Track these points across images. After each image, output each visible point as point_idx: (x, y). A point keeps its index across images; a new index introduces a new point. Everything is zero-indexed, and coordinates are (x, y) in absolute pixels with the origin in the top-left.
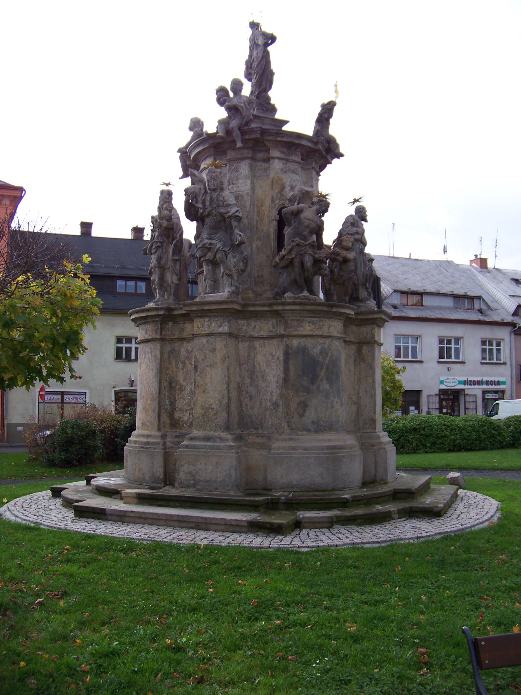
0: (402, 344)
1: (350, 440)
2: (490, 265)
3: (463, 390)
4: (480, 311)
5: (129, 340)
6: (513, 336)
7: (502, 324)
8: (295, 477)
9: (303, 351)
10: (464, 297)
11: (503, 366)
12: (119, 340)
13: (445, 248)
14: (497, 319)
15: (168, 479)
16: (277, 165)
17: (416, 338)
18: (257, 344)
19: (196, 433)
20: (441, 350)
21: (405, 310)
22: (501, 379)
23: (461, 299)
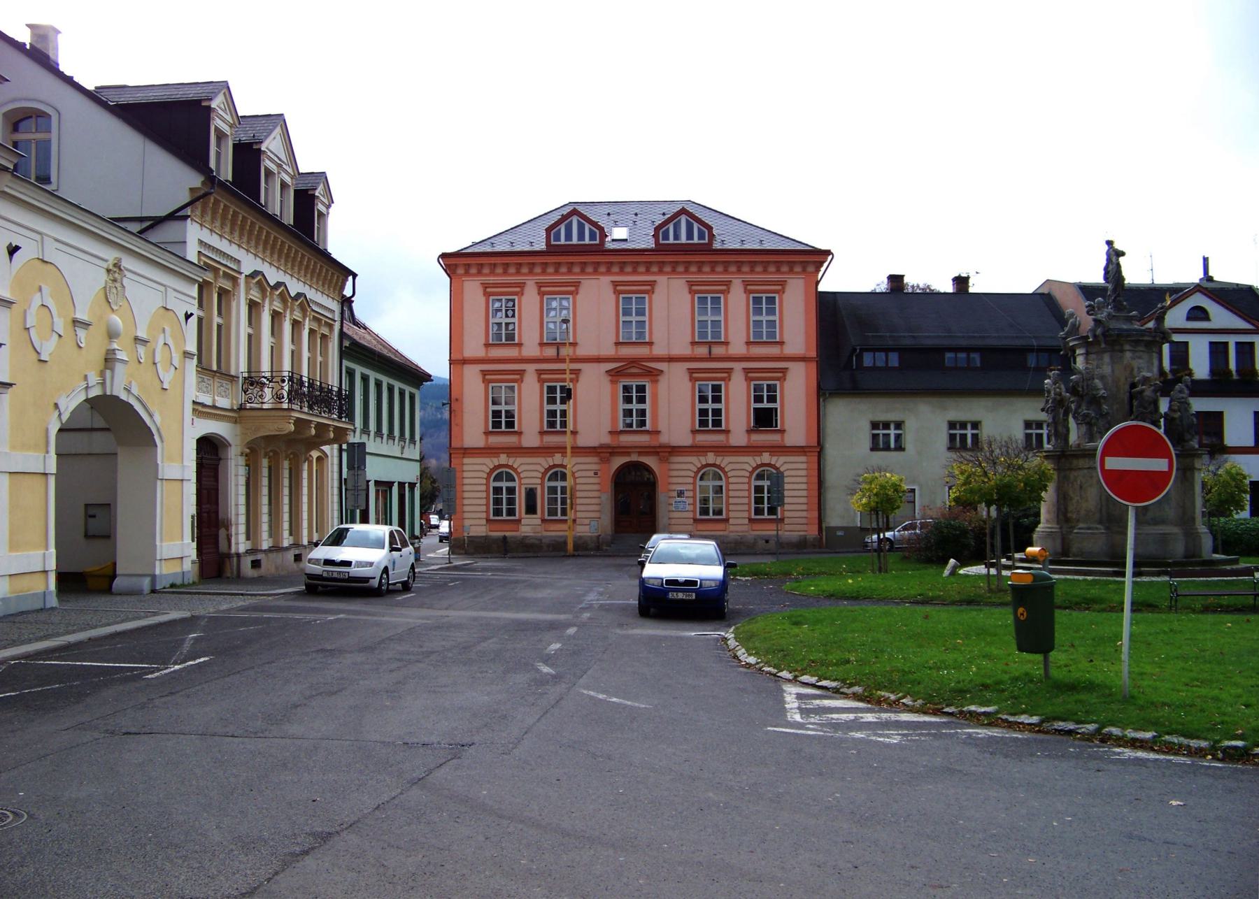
1: (1175, 530)
12: (875, 425)
15: (1065, 552)
16: (1128, 355)
19: (1081, 525)
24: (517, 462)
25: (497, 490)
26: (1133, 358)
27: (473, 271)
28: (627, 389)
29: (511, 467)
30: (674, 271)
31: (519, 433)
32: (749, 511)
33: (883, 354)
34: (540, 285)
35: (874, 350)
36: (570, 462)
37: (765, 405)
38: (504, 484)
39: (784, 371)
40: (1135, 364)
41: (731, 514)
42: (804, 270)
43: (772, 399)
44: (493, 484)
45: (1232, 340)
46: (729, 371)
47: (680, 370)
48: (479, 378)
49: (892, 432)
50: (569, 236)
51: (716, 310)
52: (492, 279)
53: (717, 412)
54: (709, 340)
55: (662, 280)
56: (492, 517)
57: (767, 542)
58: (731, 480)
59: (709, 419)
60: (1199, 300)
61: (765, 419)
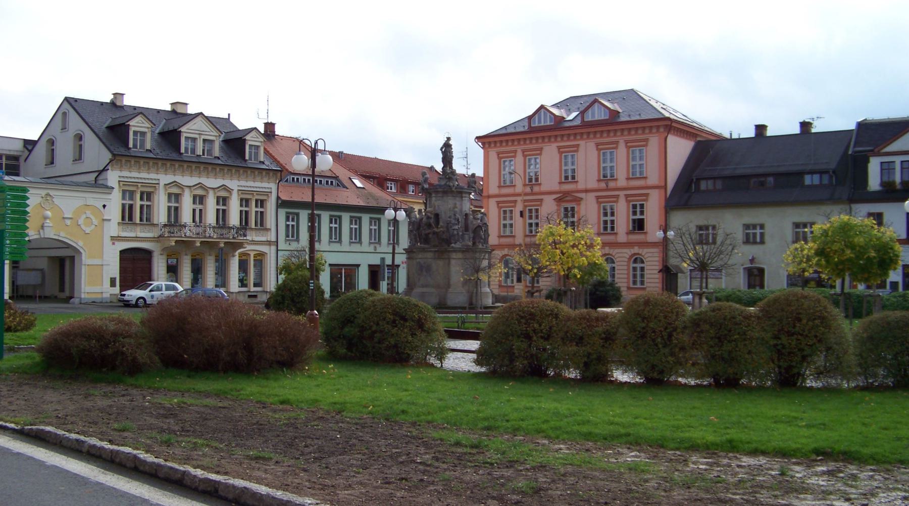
5: (754, 227)
27: (592, 136)
28: (634, 207)
30: (588, 137)
31: (616, 234)
32: (628, 282)
34: (627, 142)
35: (707, 179)
36: (645, 252)
37: (638, 216)
38: (638, 265)
39: (647, 195)
42: (658, 131)
43: (642, 213)
46: (617, 196)
47: (591, 197)
48: (594, 201)
49: (758, 231)
50: (540, 121)
52: (601, 140)
53: (612, 222)
54: (606, 178)
55: (582, 143)
59: (608, 227)
61: (639, 225)
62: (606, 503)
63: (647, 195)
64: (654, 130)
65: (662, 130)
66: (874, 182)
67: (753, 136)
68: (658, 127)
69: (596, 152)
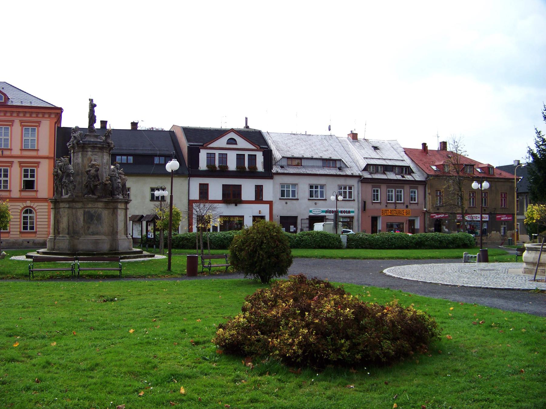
0: (285, 189)
2: (359, 137)
3: (325, 216)
4: (340, 169)
6: (360, 184)
7: (352, 176)
8: (84, 248)
9: (89, 212)
10: (330, 160)
11: (353, 202)
13: (330, 126)
14: (349, 173)
16: (90, 153)
17: (295, 185)
18: (78, 210)
20: (311, 192)
21: (288, 169)
22: (351, 210)
23: (328, 162)
24: (35, 205)
25: (25, 218)
26: (92, 155)
28: (26, 171)
29: (32, 207)
31: (10, 191)
32: (20, 228)
33: (125, 157)
34: (21, 122)
38: (29, 215)
39: (38, 163)
40: (93, 158)
41: (11, 230)
42: (49, 117)
43: (32, 176)
44: (23, 215)
45: (246, 154)
46: (12, 163)
51: (33, 135)
56: (22, 230)
57: (28, 242)
58: (38, 214)
60: (232, 135)
61: (29, 185)
62: (253, 400)
63: (38, 163)
64: (47, 116)
65: (53, 116)
66: (203, 165)
67: (130, 128)
68: (50, 114)
69: (20, 128)
